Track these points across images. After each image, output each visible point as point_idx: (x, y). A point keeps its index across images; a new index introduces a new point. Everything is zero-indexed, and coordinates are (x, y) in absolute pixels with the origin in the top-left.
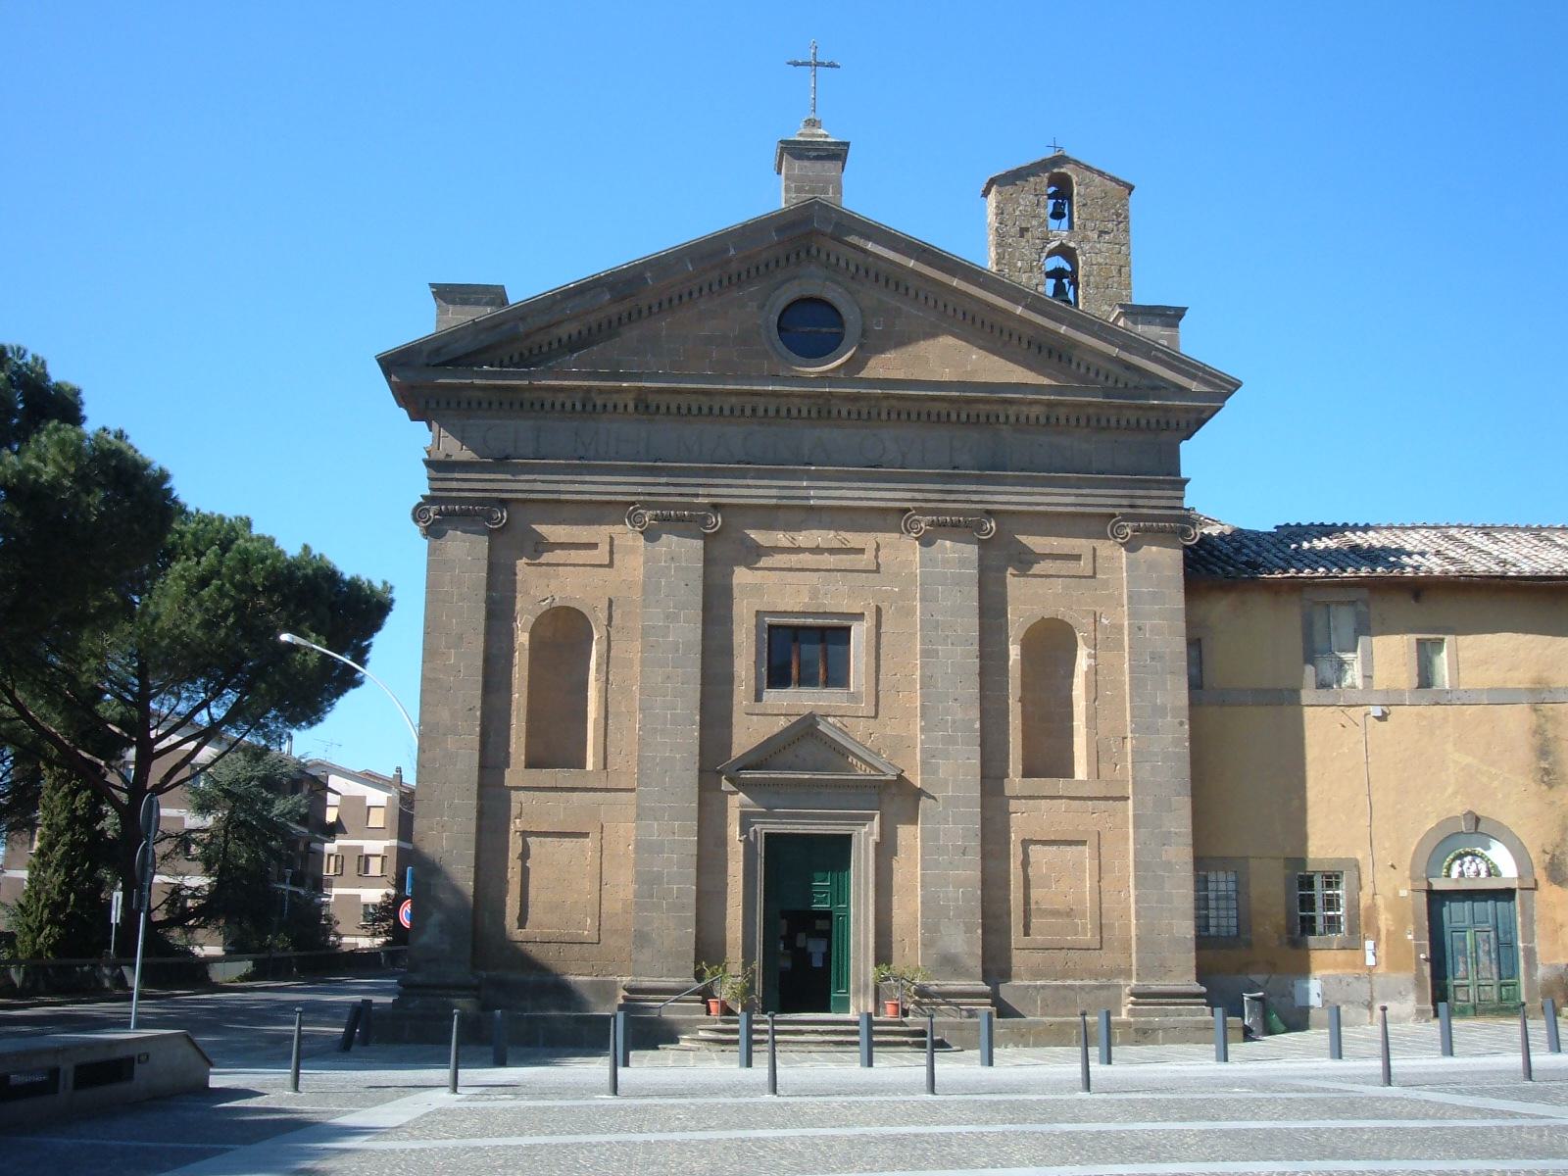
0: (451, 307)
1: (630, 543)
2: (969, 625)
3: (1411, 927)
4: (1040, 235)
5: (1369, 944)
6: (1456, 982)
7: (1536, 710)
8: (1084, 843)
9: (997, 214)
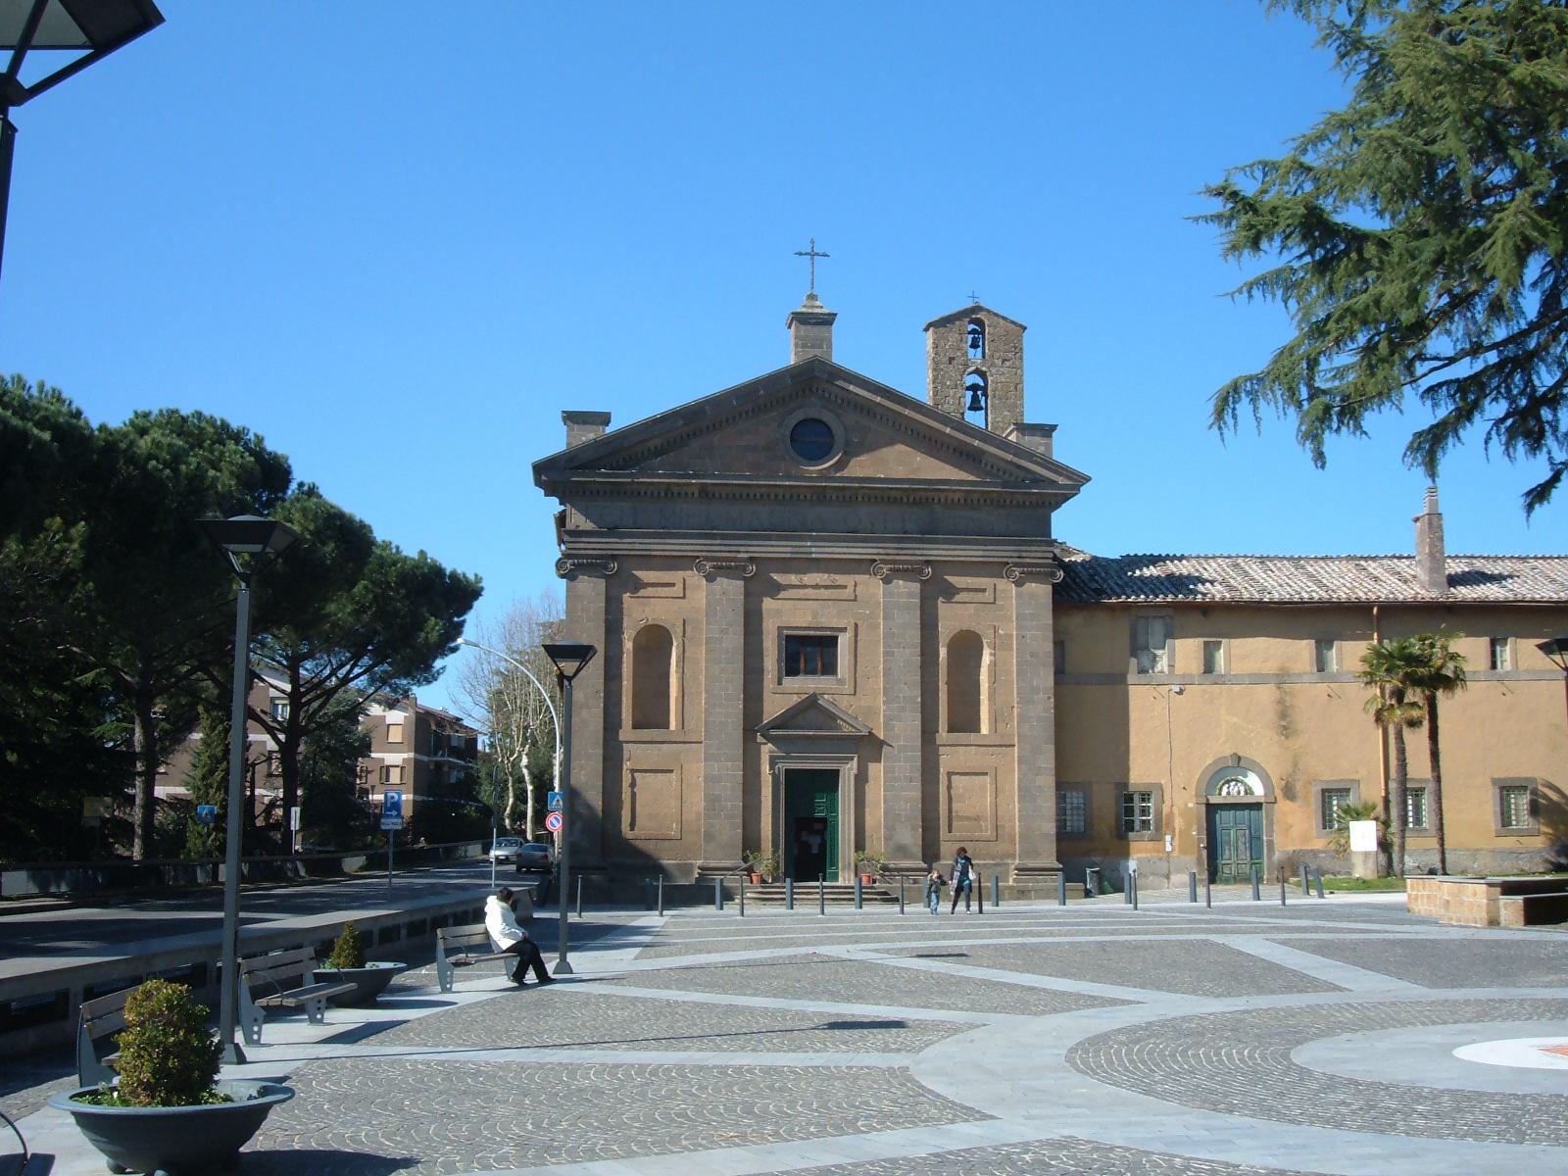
1: (697, 583)
2: (914, 635)
3: (1195, 827)
5: (1168, 838)
6: (1223, 862)
7: (1279, 688)
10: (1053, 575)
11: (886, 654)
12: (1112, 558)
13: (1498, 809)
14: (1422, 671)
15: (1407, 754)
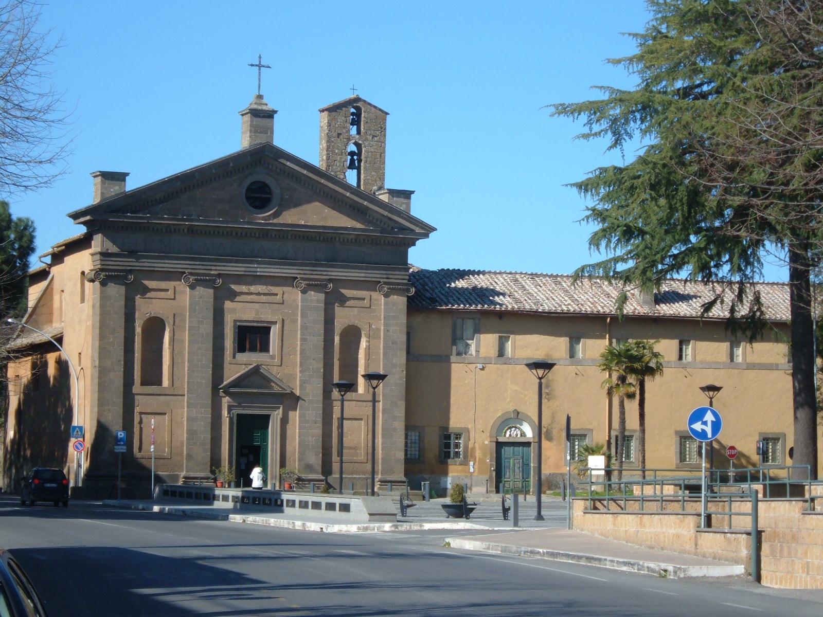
0: (107, 181)
1: (182, 289)
2: (320, 328)
3: (489, 457)
4: (346, 137)
5: (471, 463)
6: (505, 480)
8: (362, 419)
9: (328, 126)
10: (408, 290)
11: (302, 340)
12: (431, 270)
13: (678, 450)
14: (637, 365)
15: (626, 416)
